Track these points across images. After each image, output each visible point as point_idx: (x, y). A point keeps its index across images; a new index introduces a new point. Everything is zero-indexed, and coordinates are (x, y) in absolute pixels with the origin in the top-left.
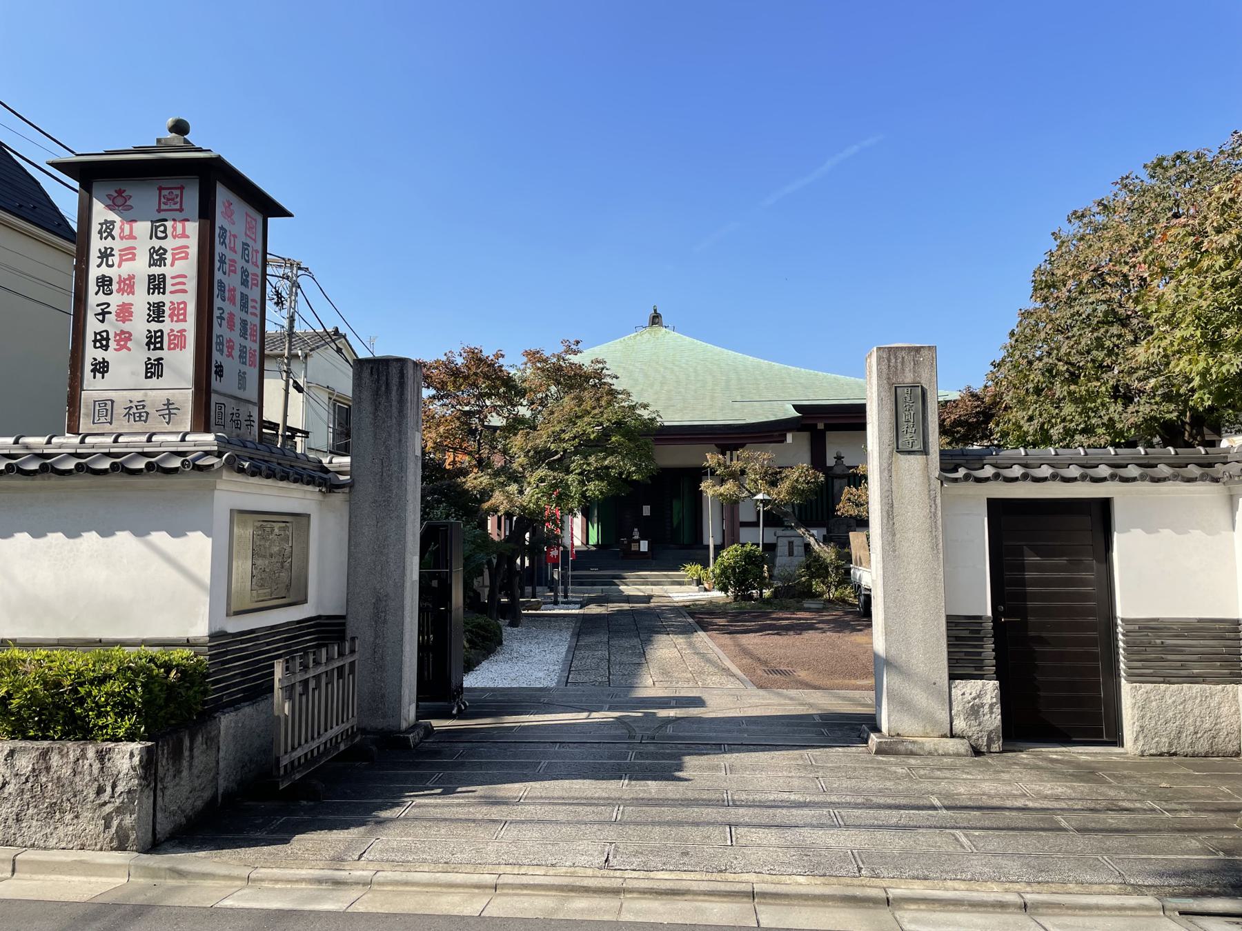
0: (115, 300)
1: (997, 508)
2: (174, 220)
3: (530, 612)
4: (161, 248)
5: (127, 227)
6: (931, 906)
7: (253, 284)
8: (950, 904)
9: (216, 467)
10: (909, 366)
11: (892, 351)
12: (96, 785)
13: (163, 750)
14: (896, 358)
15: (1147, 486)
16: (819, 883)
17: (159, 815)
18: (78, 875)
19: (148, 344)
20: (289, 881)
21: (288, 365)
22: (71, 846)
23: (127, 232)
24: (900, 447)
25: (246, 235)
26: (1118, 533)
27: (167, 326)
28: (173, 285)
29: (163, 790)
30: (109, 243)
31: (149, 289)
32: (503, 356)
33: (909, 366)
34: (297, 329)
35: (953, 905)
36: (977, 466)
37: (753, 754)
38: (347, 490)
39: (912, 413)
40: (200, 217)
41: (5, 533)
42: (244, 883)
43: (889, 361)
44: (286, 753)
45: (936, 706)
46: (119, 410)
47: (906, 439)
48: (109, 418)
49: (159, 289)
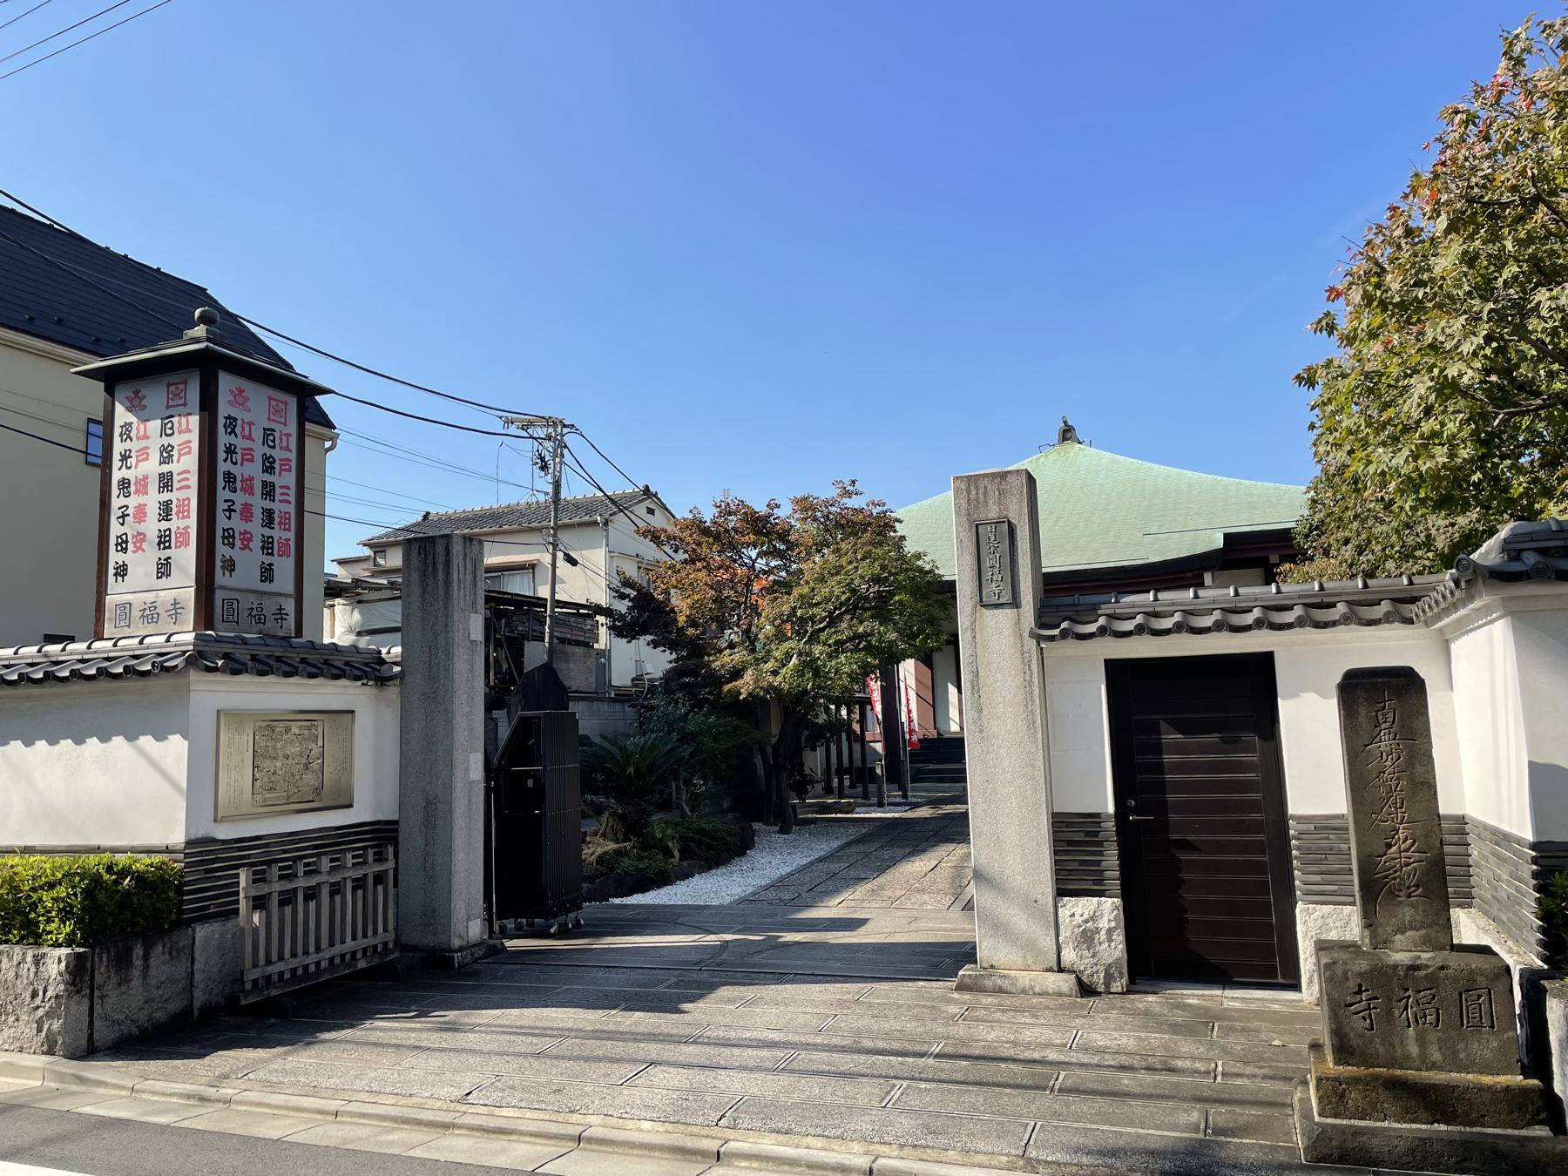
0: (133, 501)
1: (1117, 671)
2: (179, 415)
3: (839, 815)
4: (169, 445)
5: (142, 426)
6: (763, 1165)
7: (281, 470)
8: (786, 1164)
9: (180, 667)
10: (993, 497)
11: (972, 480)
12: (31, 988)
13: (101, 958)
14: (977, 488)
15: (1310, 634)
16: (661, 1130)
17: (97, 1023)
18: (7, 1076)
19: (159, 544)
20: (164, 1094)
21: (555, 535)
22: (12, 1048)
23: (142, 433)
24: (984, 599)
25: (269, 419)
26: (1282, 699)
27: (175, 524)
28: (179, 481)
29: (102, 997)
30: (128, 445)
31: (160, 487)
32: (778, 506)
33: (993, 497)
34: (565, 494)
35: (789, 1164)
36: (1092, 619)
37: (804, 986)
38: (398, 682)
39: (998, 556)
40: (200, 410)
41: (0, 740)
42: (573, 1145)
43: (969, 493)
44: (255, 966)
45: (1038, 931)
46: (136, 613)
47: (991, 589)
48: (127, 621)
49: (168, 486)
